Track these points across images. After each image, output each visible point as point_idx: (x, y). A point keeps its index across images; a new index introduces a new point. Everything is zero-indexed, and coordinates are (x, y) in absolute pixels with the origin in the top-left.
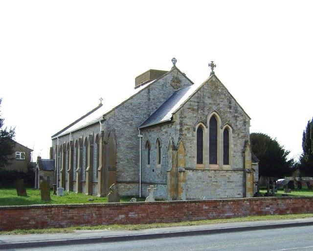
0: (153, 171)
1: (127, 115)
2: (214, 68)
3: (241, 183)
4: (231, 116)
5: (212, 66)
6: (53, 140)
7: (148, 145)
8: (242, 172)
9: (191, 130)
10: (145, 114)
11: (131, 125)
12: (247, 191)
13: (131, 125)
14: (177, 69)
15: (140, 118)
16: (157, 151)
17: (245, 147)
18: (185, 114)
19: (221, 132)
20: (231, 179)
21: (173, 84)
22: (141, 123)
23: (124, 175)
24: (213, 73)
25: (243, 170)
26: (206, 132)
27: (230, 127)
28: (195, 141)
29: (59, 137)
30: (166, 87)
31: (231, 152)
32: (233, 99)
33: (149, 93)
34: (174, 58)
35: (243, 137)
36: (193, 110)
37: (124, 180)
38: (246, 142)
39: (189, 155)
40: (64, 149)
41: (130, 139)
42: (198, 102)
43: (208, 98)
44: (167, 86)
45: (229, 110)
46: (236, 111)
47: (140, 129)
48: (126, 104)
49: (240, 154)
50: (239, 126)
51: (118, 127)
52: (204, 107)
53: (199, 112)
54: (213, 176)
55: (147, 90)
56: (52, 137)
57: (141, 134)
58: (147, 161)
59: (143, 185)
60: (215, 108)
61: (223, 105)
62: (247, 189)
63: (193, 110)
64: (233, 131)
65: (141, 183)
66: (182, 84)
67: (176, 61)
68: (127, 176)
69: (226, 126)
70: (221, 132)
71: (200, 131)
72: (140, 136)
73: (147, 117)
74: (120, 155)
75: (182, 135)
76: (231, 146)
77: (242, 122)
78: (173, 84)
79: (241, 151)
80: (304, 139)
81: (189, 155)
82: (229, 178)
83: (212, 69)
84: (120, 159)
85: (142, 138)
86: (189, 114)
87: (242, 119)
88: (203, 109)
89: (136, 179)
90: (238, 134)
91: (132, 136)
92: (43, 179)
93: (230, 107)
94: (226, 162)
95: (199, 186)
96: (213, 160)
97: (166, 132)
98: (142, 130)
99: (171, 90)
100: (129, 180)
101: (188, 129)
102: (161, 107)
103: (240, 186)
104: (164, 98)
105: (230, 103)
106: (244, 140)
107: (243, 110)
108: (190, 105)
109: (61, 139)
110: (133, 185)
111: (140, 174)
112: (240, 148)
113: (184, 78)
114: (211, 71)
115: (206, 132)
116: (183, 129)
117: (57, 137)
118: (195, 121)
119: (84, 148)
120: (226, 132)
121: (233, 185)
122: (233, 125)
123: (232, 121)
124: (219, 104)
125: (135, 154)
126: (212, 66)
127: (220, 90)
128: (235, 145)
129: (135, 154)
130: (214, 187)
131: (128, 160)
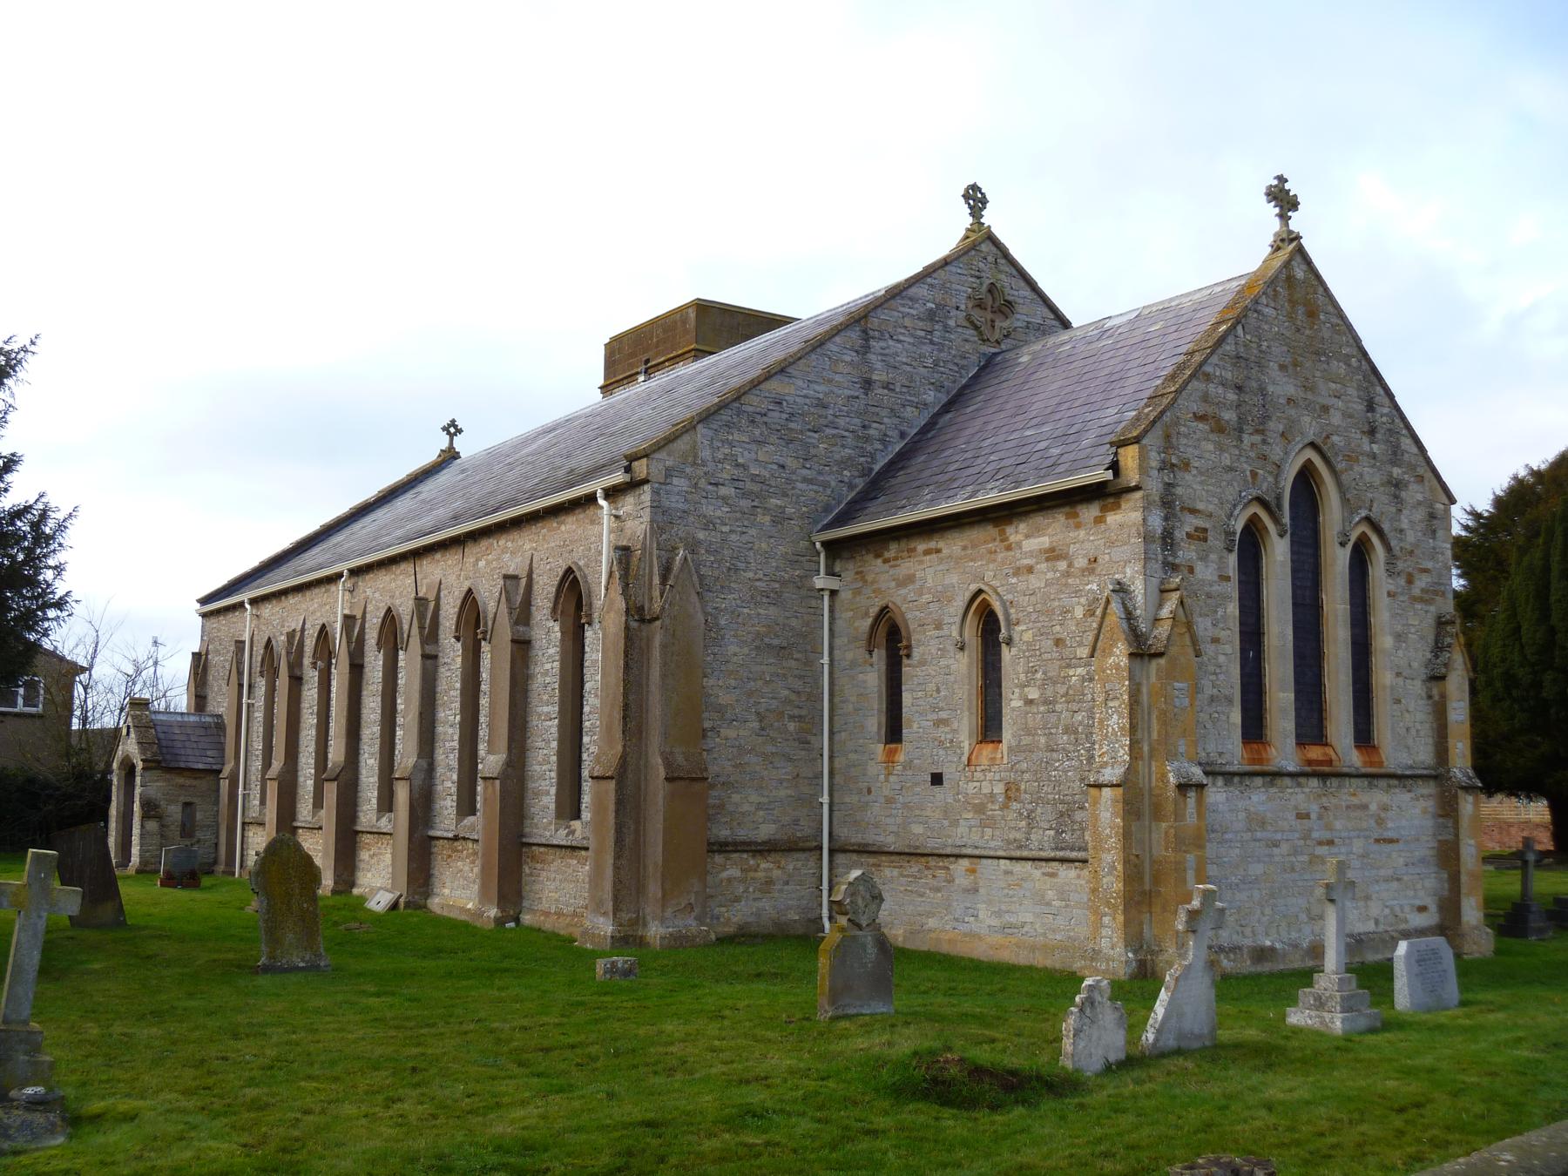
0: (937, 779)
1: (761, 458)
3: (1425, 848)
4: (1377, 480)
5: (1283, 199)
6: (204, 615)
7: (891, 638)
8: (1429, 789)
9: (1216, 541)
10: (844, 463)
11: (779, 519)
12: (1464, 890)
13: (779, 519)
14: (991, 239)
15: (825, 485)
16: (963, 667)
17: (1439, 648)
18: (1186, 447)
19: (1337, 562)
21: (977, 315)
22: (827, 509)
23: (744, 801)
24: (1289, 242)
25: (1438, 775)
26: (1278, 552)
27: (1375, 539)
28: (1233, 609)
29: (253, 602)
30: (946, 328)
31: (1383, 678)
32: (1379, 390)
33: (866, 349)
34: (975, 187)
36: (1219, 428)
37: (743, 834)
38: (1441, 623)
39: (1209, 691)
40: (283, 665)
41: (775, 599)
42: (1239, 388)
44: (952, 323)
46: (1396, 456)
47: (824, 544)
48: (754, 402)
49: (1417, 687)
51: (709, 525)
52: (1265, 418)
54: (1314, 809)
55: (854, 335)
56: (204, 601)
57: (830, 572)
58: (874, 722)
59: (841, 859)
60: (1310, 428)
61: (1342, 419)
62: (1464, 878)
65: (832, 852)
66: (1018, 320)
67: (984, 201)
68: (755, 810)
70: (1337, 562)
71: (1250, 546)
72: (820, 582)
73: (860, 483)
74: (722, 690)
75: (1174, 568)
76: (1383, 641)
77: (1420, 515)
78: (977, 315)
79: (1423, 673)
81: (1209, 691)
83: (1284, 217)
84: (720, 710)
85: (833, 593)
86: (1201, 448)
87: (1420, 497)
89: (805, 829)
90: (1410, 581)
91: (784, 583)
92: (159, 817)
93: (1372, 432)
94: (1364, 736)
95: (1256, 869)
96: (1311, 727)
97: (1052, 555)
98: (835, 549)
99: (966, 347)
100: (766, 831)
101: (1200, 535)
102: (925, 430)
103: (1423, 861)
104: (939, 387)
105: (1371, 407)
107: (1422, 449)
108: (1205, 398)
109: (267, 610)
110: (791, 863)
111: (825, 799)
112: (1417, 654)
113: (1027, 293)
114: (1276, 225)
115: (1278, 552)
117: (244, 596)
118: (1230, 494)
119: (312, 676)
122: (1386, 526)
123: (1382, 507)
125: (798, 685)
126: (1283, 199)
127: (1326, 334)
129: (798, 685)
131: (760, 717)
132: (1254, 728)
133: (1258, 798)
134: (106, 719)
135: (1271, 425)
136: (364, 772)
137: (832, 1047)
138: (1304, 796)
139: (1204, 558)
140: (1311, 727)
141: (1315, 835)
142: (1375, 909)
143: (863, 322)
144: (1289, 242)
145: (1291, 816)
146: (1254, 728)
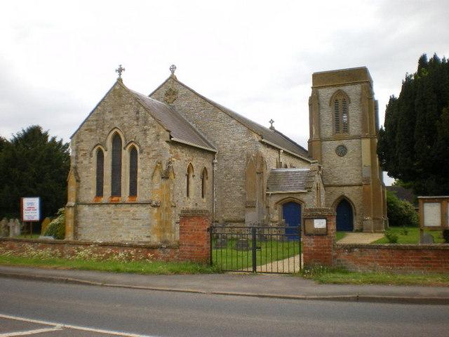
2: (123, 73)
20: (137, 216)
24: (120, 81)
42: (96, 120)
50: (150, 142)
54: (113, 211)
88: (102, 129)
94: (133, 192)
96: (116, 191)
101: (85, 155)
105: (138, 113)
132: (100, 193)
133: (97, 209)
134: (239, 136)
135: (105, 126)
136: (110, 183)
137: (389, 244)
138: (111, 209)
139: (85, 159)
140: (116, 191)
141: (113, 217)
142: (131, 236)
143: (128, 91)
144: (120, 81)
145: (106, 213)
146: (100, 193)
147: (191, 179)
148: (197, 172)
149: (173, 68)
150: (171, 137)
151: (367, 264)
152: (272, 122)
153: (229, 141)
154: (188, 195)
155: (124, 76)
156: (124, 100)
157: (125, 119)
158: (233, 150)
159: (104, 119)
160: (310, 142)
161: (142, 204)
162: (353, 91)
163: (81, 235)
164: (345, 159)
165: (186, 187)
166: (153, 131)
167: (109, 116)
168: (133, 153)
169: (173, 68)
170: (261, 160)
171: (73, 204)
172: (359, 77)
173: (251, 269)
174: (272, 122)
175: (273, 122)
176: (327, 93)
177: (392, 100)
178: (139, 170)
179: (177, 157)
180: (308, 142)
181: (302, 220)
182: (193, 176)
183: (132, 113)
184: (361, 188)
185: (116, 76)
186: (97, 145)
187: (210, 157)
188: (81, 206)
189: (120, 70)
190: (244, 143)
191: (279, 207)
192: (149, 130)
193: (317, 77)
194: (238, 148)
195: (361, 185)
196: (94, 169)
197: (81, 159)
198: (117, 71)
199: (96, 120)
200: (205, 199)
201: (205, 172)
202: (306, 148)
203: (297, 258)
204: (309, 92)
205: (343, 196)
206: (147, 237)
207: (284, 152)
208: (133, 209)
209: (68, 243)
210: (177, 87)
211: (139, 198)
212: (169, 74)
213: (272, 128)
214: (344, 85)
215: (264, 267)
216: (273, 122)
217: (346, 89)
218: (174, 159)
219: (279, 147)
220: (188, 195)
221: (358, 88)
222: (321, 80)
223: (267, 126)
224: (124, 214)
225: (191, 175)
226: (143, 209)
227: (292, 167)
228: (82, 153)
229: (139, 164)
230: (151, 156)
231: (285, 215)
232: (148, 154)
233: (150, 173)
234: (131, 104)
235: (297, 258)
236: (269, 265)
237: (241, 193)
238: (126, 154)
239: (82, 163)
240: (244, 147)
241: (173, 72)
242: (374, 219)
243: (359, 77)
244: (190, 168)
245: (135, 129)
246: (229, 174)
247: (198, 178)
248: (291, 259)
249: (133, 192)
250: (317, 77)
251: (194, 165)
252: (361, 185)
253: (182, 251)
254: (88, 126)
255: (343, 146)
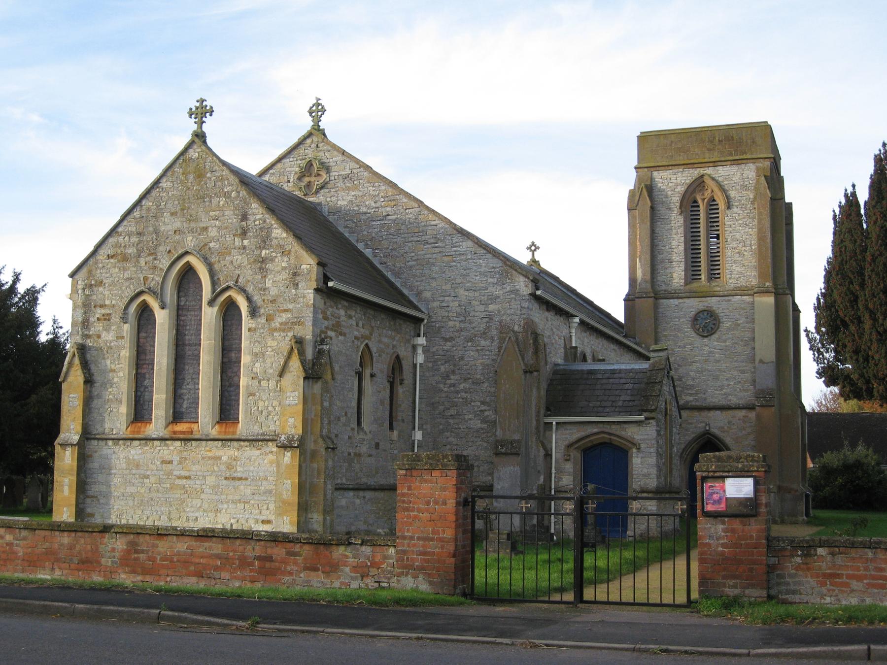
2: (208, 119)
9: (116, 318)
20: (240, 472)
24: (200, 137)
35: (286, 326)
42: (140, 234)
43: (172, 214)
45: (238, 242)
50: (274, 291)
53: (142, 262)
54: (176, 459)
63: (125, 258)
64: (254, 312)
69: (557, 441)
77: (284, 275)
80: (629, 199)
82: (229, 467)
88: (153, 254)
94: (227, 411)
101: (107, 318)
105: (244, 217)
106: (290, 334)
114: (195, 127)
115: (162, 318)
116: (92, 319)
120: (229, 312)
121: (245, 489)
123: (248, 275)
124: (205, 229)
128: (256, 355)
130: (178, 494)
132: (140, 412)
135: (161, 248)
139: (107, 330)
146: (140, 412)
147: (367, 383)
148: (381, 366)
149: (317, 110)
150: (326, 279)
151: (847, 585)
152: (533, 248)
153: (438, 292)
154: (359, 423)
155: (210, 126)
156: (210, 184)
157: (213, 233)
158: (465, 315)
159: (156, 232)
160: (629, 300)
161: (254, 441)
162: (738, 179)
163: (92, 515)
164: (714, 343)
165: (354, 403)
166: (281, 262)
167: (169, 224)
168: (229, 312)
169: (317, 110)
170: (534, 339)
171: (76, 438)
172: (753, 144)
173: (569, 597)
174: (533, 248)
175: (537, 248)
176: (673, 183)
177: (866, 202)
178: (245, 359)
179: (337, 327)
180: (625, 300)
181: (698, 481)
182: (372, 376)
183: (231, 218)
184: (752, 415)
185: (191, 126)
186: (141, 293)
187: (408, 328)
188: (95, 443)
189: (201, 112)
190: (493, 299)
191: (576, 455)
192: (272, 260)
193: (646, 140)
194: (479, 310)
195: (750, 408)
196: (126, 353)
197: (97, 327)
198: (211, 112)
199: (140, 234)
200: (395, 432)
201: (397, 365)
202: (619, 315)
203: (681, 562)
204: (629, 180)
205: (707, 433)
206: (263, 522)
207: (582, 322)
208: (227, 453)
209: (59, 528)
210: (333, 159)
211: (243, 427)
212: (307, 123)
213: (535, 262)
214: (715, 164)
215: (602, 589)
216: (537, 248)
217: (722, 172)
218: (331, 333)
219: (571, 311)
220: (359, 423)
221: (749, 172)
222: (659, 148)
223: (524, 258)
224: (206, 461)
225: (368, 372)
226: (252, 452)
227: (595, 360)
228: (99, 312)
229: (244, 344)
230: (276, 324)
231: (587, 474)
232: (269, 319)
233: (274, 362)
234: (227, 195)
235: (681, 562)
236: (614, 586)
237: (484, 421)
238: (209, 316)
239: (99, 336)
240: (491, 307)
241: (317, 121)
242: (780, 488)
243: (753, 144)
244: (367, 356)
245: (238, 258)
246: (453, 372)
247: (382, 381)
248: (667, 565)
249: (227, 411)
250: (646, 140)
251: (374, 350)
252: (750, 408)
253: (405, 552)
254: (117, 245)
255: (710, 314)
